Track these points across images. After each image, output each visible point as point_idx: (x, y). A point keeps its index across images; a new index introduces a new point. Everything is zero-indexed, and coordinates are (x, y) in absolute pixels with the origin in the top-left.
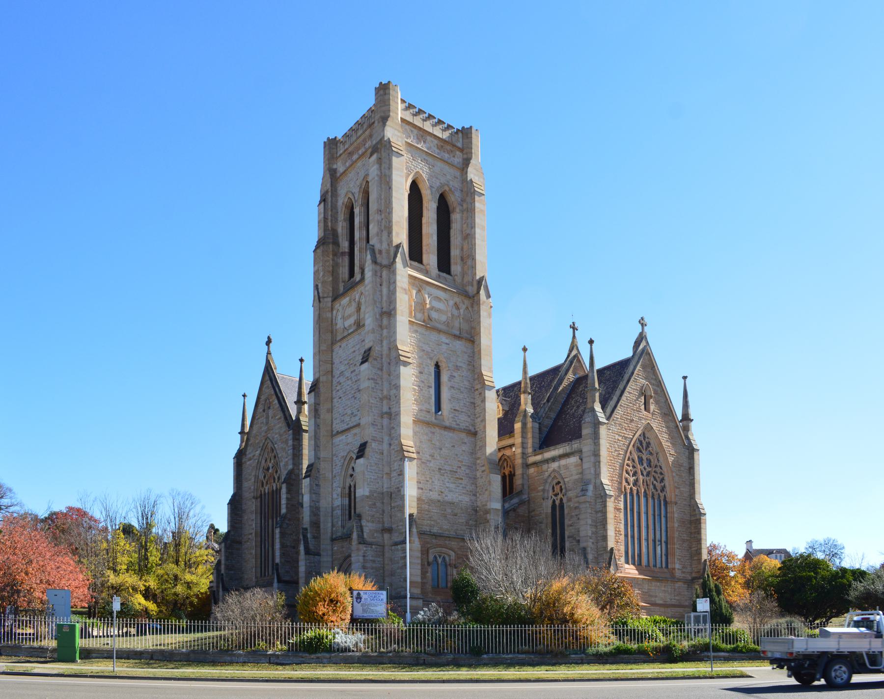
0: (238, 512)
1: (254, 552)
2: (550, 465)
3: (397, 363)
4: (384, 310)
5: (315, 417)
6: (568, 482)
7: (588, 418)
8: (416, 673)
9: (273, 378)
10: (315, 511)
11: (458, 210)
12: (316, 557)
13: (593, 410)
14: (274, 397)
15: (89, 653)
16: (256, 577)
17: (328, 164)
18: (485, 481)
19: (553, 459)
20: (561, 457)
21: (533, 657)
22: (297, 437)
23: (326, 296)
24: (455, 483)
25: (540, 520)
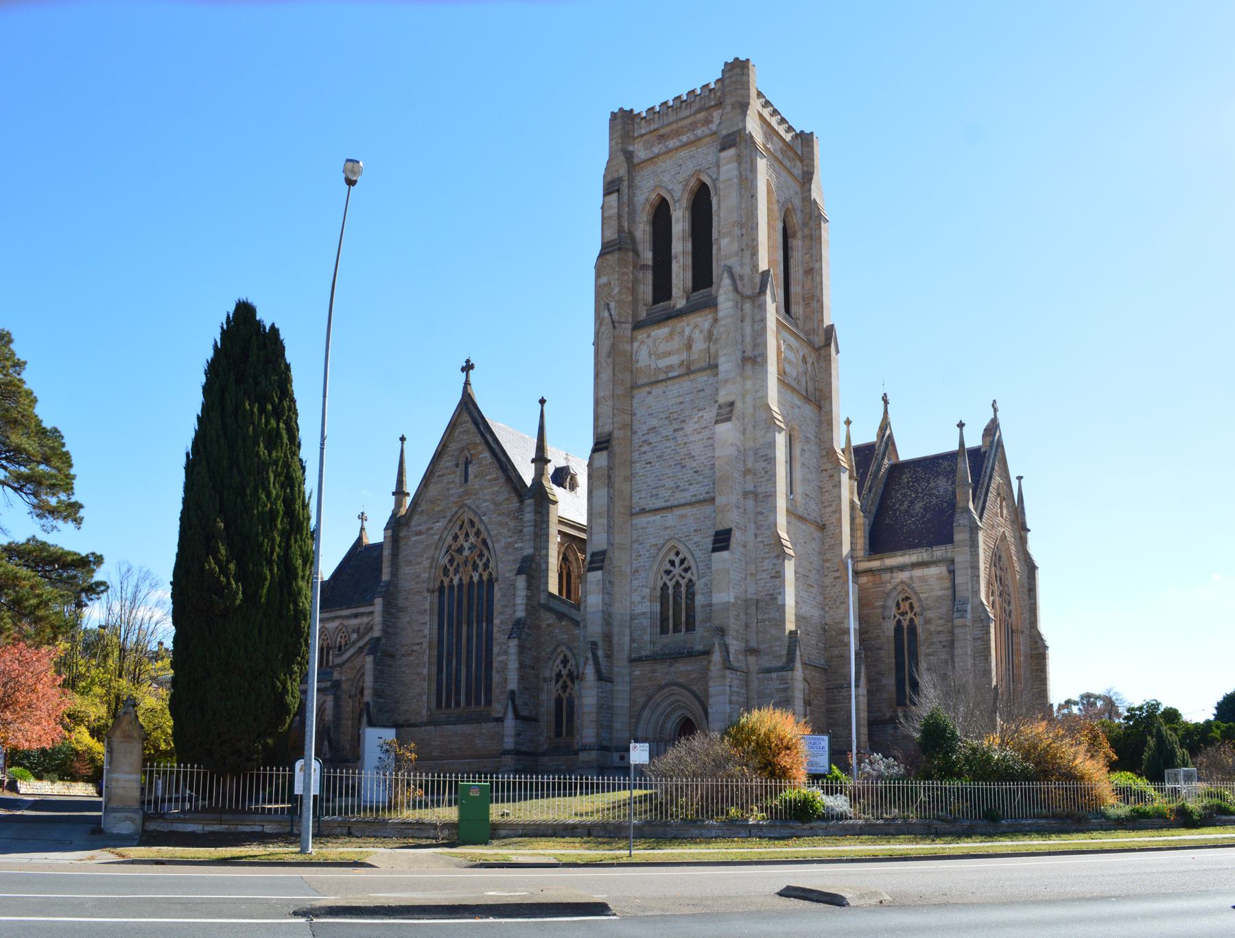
0: (392, 611)
1: (425, 671)
2: (895, 575)
3: (770, 427)
4: (748, 354)
7: (961, 520)
10: (607, 618)
11: (799, 234)
12: (608, 684)
14: (482, 447)
15: (495, 830)
16: (429, 709)
17: (622, 143)
19: (902, 568)
20: (914, 566)
21: (1053, 822)
23: (623, 320)
24: (807, 592)
25: (877, 646)
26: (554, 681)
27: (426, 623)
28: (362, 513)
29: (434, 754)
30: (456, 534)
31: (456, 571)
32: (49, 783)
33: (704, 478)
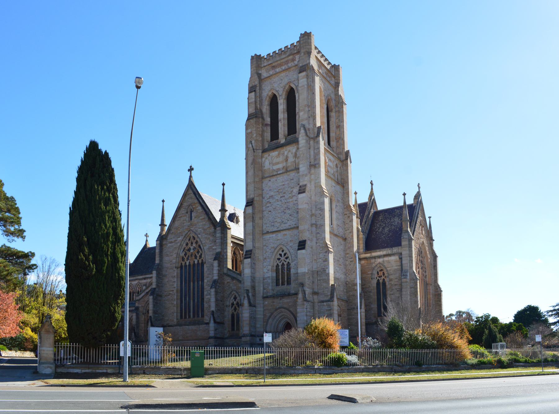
0: (160, 276)
1: (175, 303)
2: (376, 260)
4: (312, 163)
6: (390, 270)
7: (404, 236)
8: (403, 377)
9: (196, 192)
10: (253, 279)
11: (334, 110)
13: (408, 231)
14: (198, 205)
16: (177, 319)
18: (353, 267)
19: (379, 257)
20: (385, 256)
22: (223, 232)
23: (258, 148)
25: (369, 291)
26: (230, 307)
27: (175, 282)
28: (147, 234)
29: (180, 338)
31: (188, 259)
32: (15, 352)
33: (294, 218)
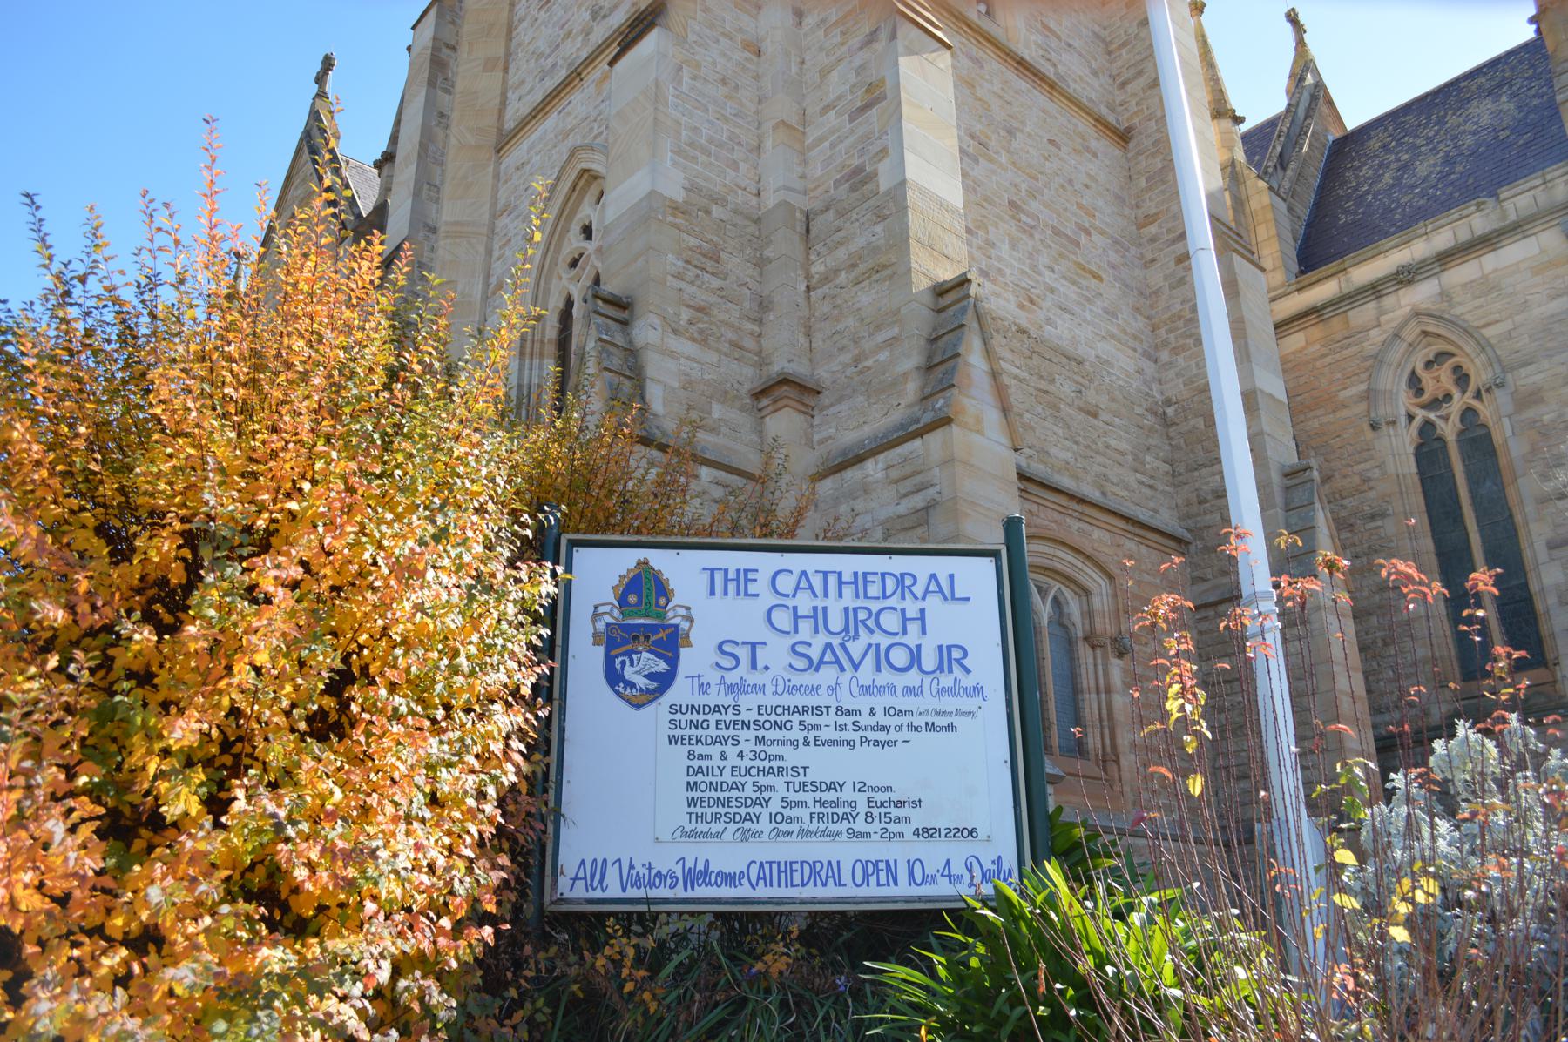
2: (1388, 301)
5: (431, 83)
6: (1509, 336)
19: (1405, 276)
20: (1444, 259)
30: (818, 687)
